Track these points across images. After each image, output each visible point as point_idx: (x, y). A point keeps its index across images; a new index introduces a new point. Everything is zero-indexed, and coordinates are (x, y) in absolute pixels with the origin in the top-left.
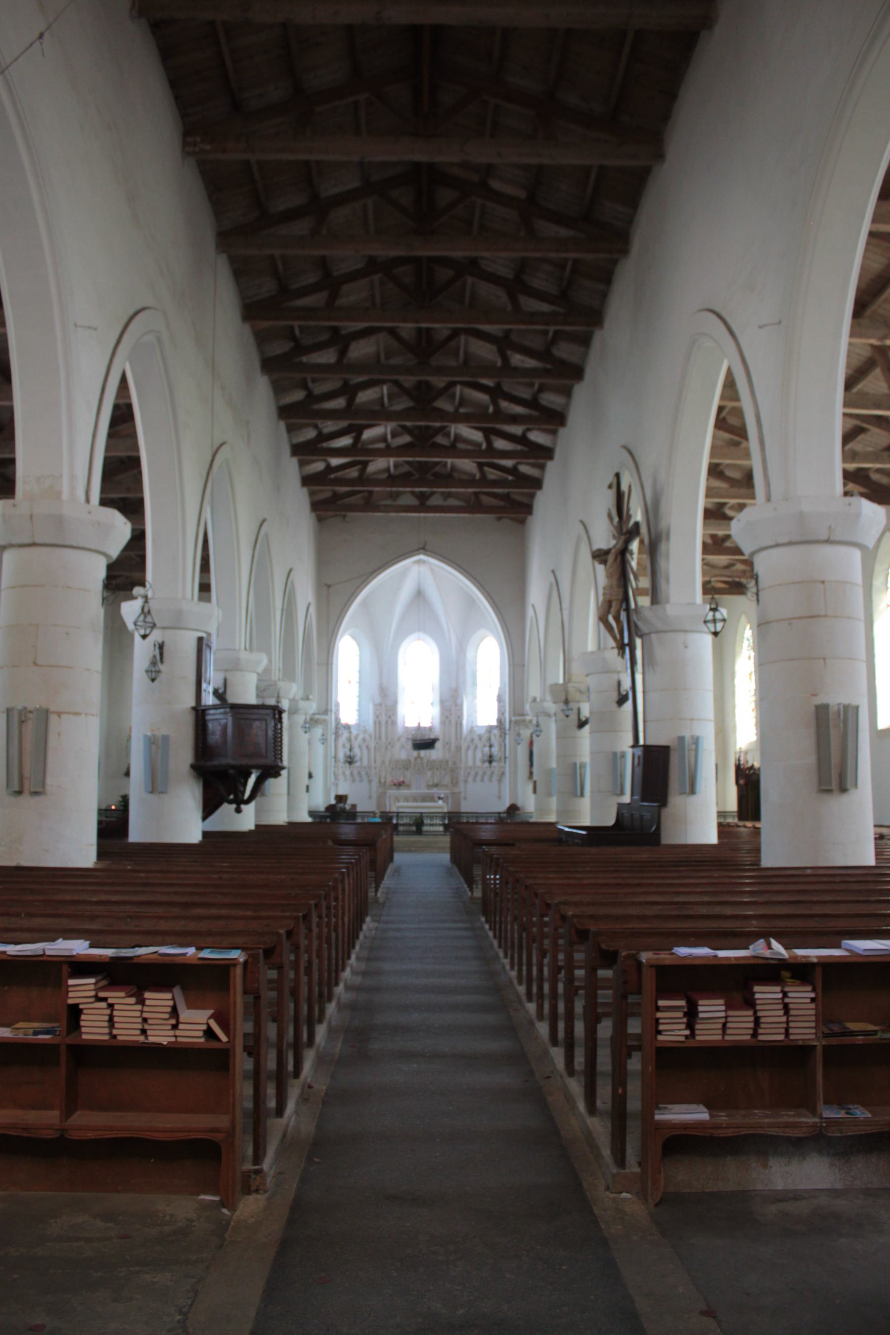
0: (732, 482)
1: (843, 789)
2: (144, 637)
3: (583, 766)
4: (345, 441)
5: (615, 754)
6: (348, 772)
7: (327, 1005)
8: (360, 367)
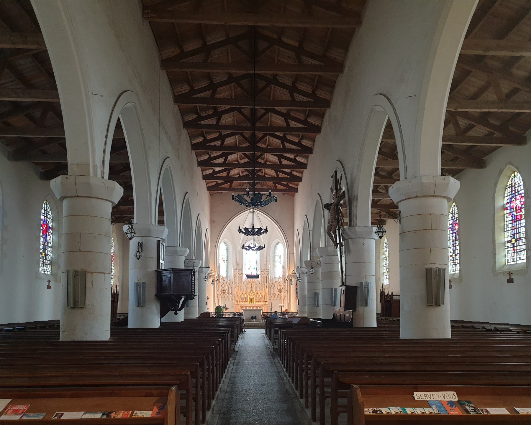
0: (387, 175)
1: (437, 304)
3: (318, 294)
4: (221, 160)
5: (332, 289)
6: (223, 297)
8: (226, 127)
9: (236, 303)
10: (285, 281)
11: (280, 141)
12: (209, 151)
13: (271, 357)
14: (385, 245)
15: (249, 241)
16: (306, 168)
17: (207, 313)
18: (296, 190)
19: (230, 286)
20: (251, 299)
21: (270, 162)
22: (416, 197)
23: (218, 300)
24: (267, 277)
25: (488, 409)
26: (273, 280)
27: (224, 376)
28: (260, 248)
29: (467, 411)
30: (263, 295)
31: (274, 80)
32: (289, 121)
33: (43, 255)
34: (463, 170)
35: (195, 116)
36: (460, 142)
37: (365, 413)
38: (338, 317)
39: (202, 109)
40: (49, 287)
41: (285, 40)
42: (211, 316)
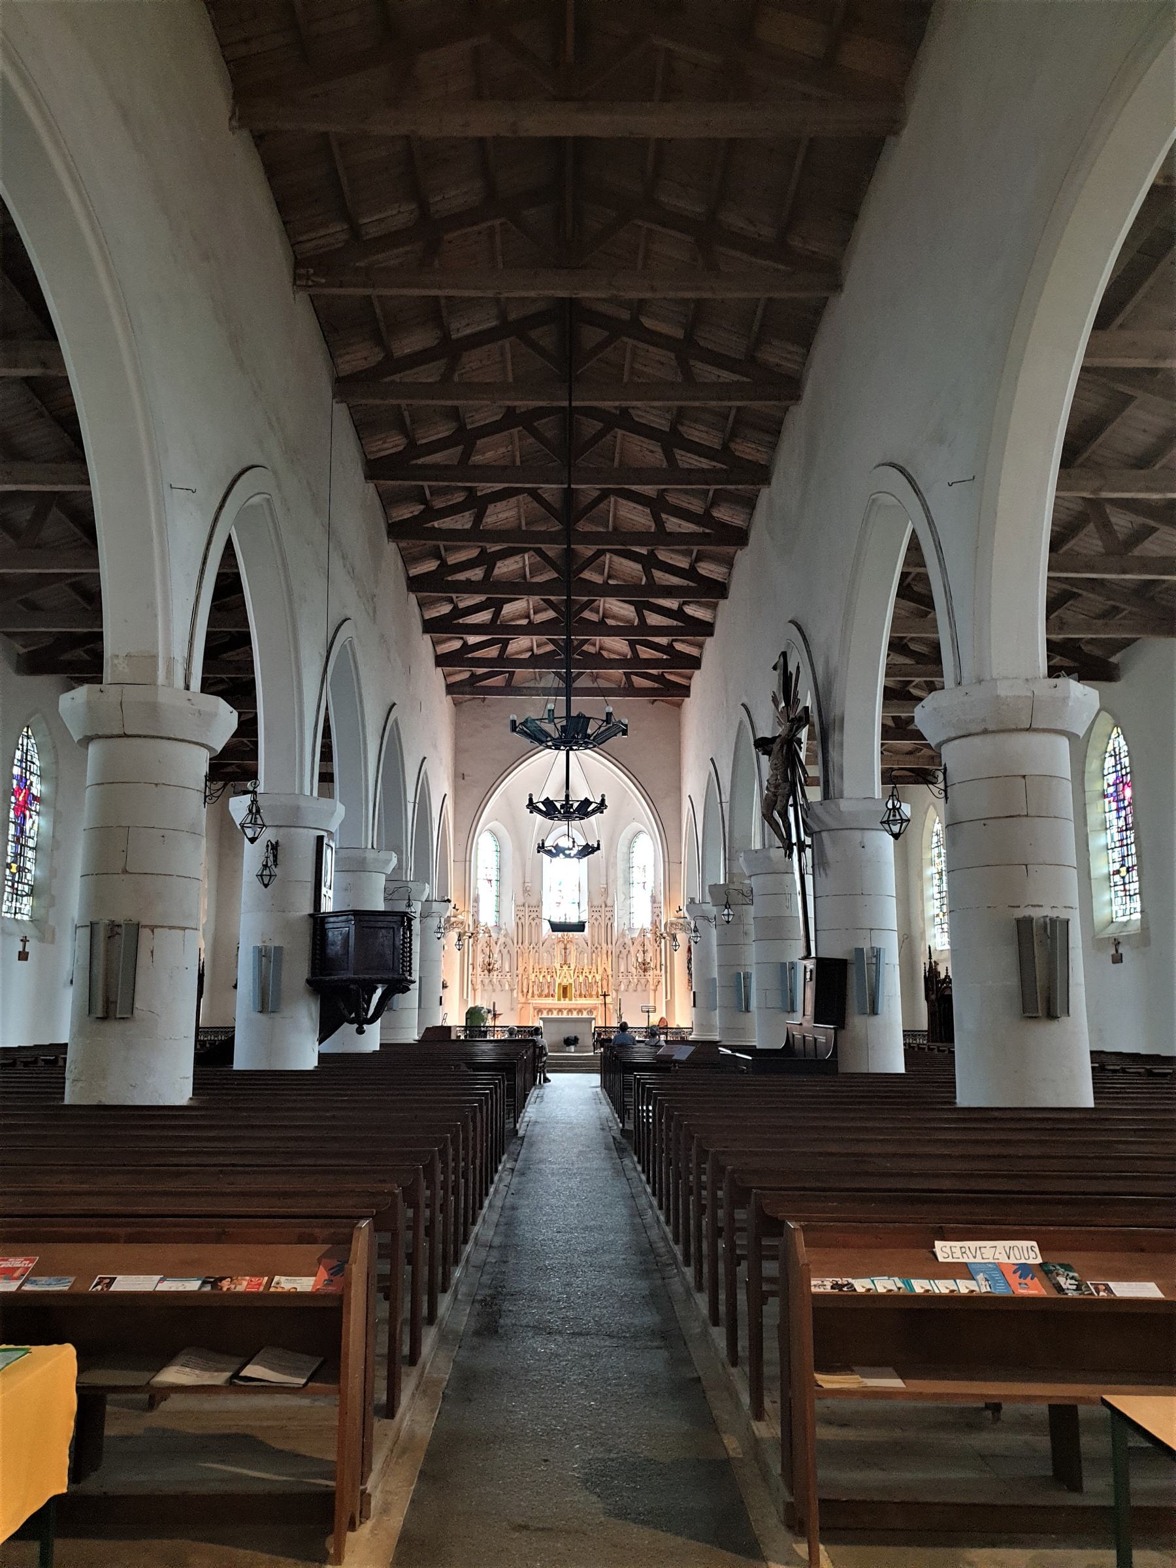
0: (917, 661)
1: (1051, 1015)
2: (252, 840)
3: (747, 976)
4: (484, 617)
5: (783, 965)
6: (486, 981)
7: (440, 1296)
9: (523, 1000)
10: (658, 937)
11: (639, 567)
12: (454, 596)
13: (615, 1154)
14: (935, 839)
15: (558, 833)
16: (712, 635)
17: (442, 1027)
18: (685, 691)
19: (505, 951)
20: (565, 989)
21: (614, 617)
22: (985, 732)
23: (474, 990)
24: (609, 927)
25: (1111, 1284)
26: (623, 935)
27: (486, 1203)
28: (588, 850)
29: (1060, 1289)
30: (598, 978)
31: (625, 420)
32: (664, 516)
33: (14, 870)
34: (1135, 640)
35: (417, 509)
36: (1116, 572)
37: (813, 1290)
38: (798, 1045)
39: (435, 492)
40: (23, 956)
41: (647, 322)
42: (453, 1037)
